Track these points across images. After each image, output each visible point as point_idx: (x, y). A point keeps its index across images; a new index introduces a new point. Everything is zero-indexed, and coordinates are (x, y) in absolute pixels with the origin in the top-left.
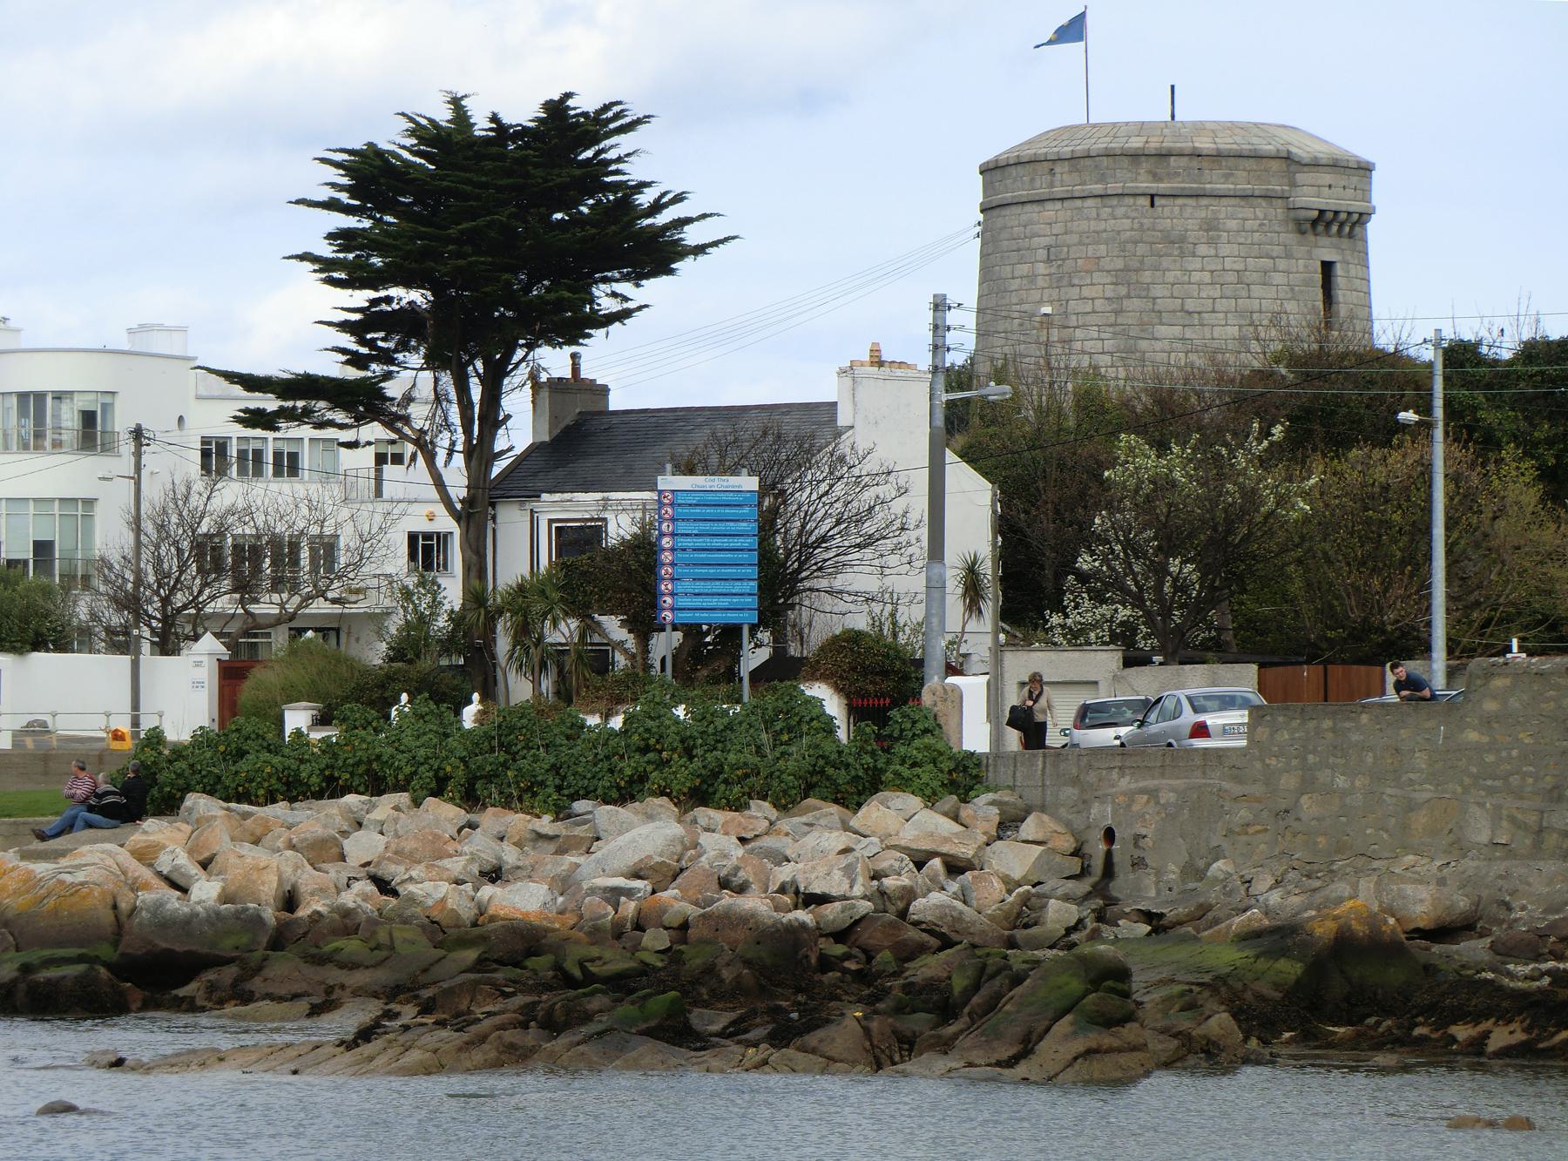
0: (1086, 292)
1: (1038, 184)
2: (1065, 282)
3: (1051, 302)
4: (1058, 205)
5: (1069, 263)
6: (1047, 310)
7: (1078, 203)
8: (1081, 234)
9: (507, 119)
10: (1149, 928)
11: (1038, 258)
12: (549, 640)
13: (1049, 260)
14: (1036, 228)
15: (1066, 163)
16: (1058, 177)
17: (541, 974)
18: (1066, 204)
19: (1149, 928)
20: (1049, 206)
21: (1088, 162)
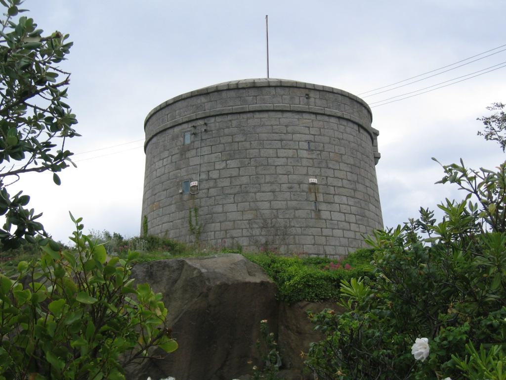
0: (337, 174)
1: (297, 101)
2: (324, 165)
3: (316, 177)
4: (313, 117)
5: (324, 154)
6: (314, 180)
7: (326, 118)
8: (330, 137)
9: (52, 238)
10: (5, 95)
11: (314, 101)
12: (481, 344)
13: (309, 150)
14: (297, 128)
15: (318, 93)
16: (312, 100)
17: (328, 257)
18: (319, 117)
19: (5, 95)
20: (305, 116)
21: (331, 96)
